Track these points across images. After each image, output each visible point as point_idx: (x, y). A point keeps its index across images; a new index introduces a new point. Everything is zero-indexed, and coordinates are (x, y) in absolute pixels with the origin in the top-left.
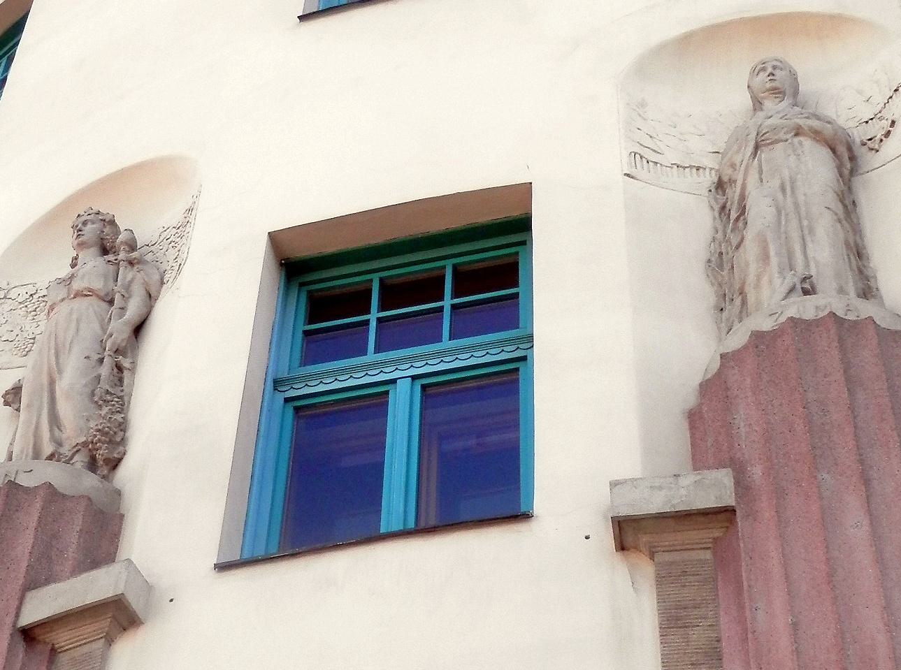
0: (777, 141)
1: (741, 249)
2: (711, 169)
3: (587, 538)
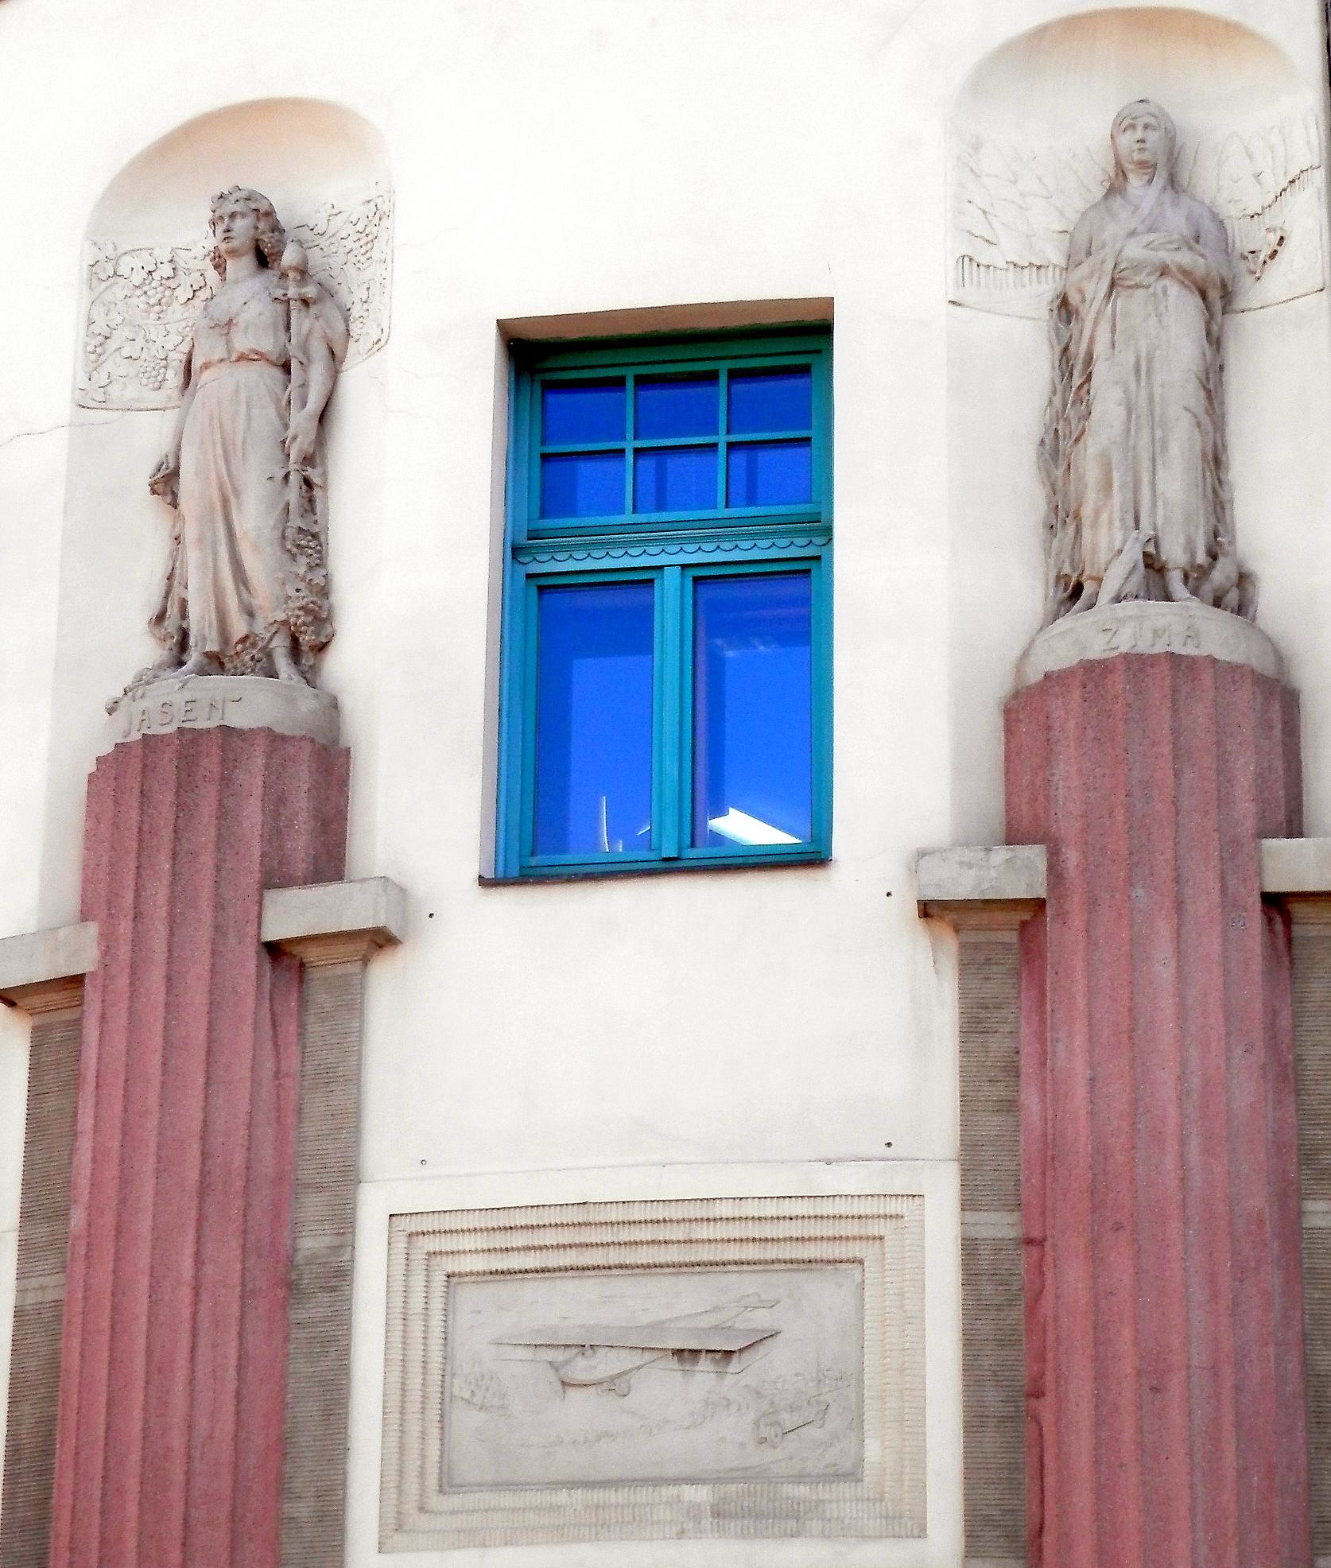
0: (1137, 286)
1: (1081, 445)
2: (1055, 266)
3: (889, 894)
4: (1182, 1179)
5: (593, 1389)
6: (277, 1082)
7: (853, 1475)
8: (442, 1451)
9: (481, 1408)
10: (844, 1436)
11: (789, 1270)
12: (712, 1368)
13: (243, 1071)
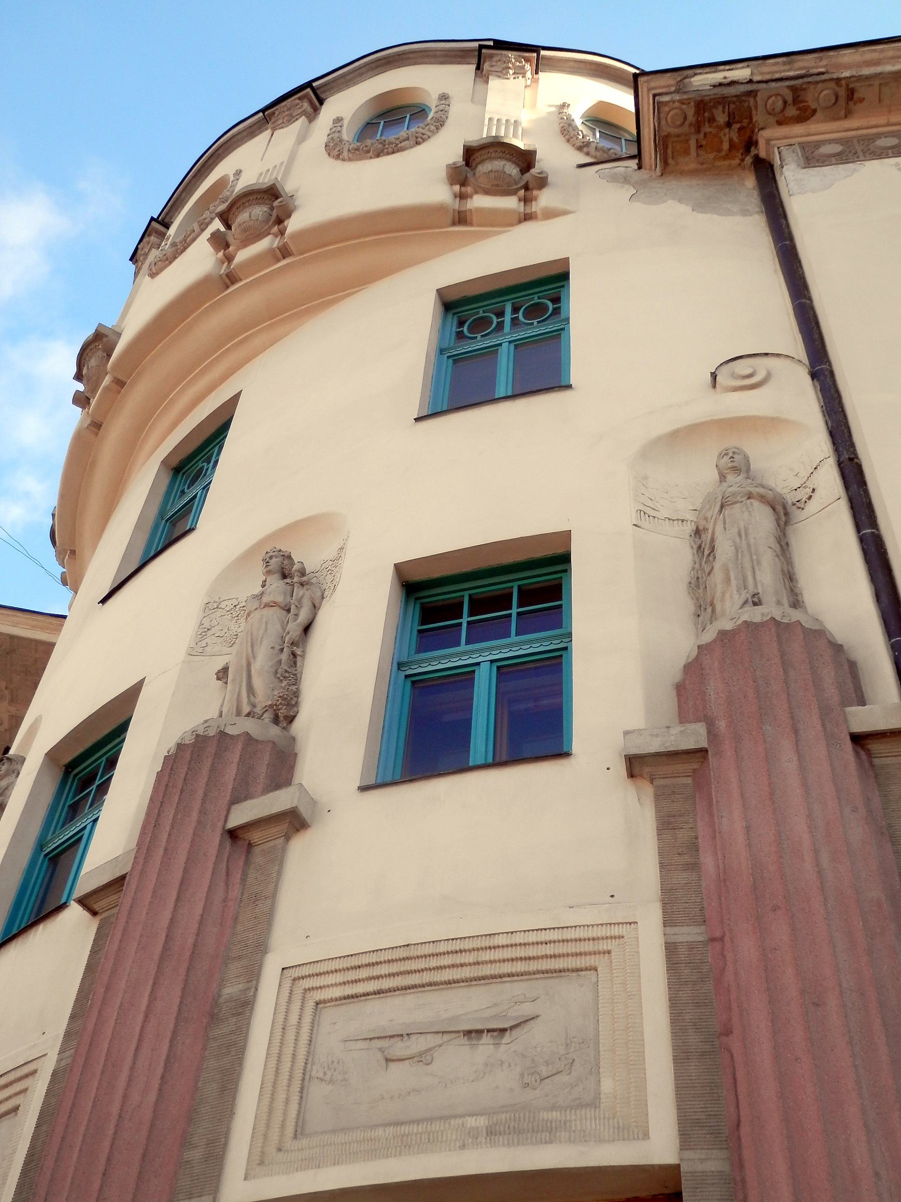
1: (712, 575)
2: (691, 521)
3: (608, 769)
4: (819, 872)
5: (407, 1062)
6: (224, 904)
7: (594, 1104)
8: (299, 1112)
9: (330, 1083)
10: (586, 1079)
11: (545, 978)
12: (491, 1041)
13: (201, 895)
